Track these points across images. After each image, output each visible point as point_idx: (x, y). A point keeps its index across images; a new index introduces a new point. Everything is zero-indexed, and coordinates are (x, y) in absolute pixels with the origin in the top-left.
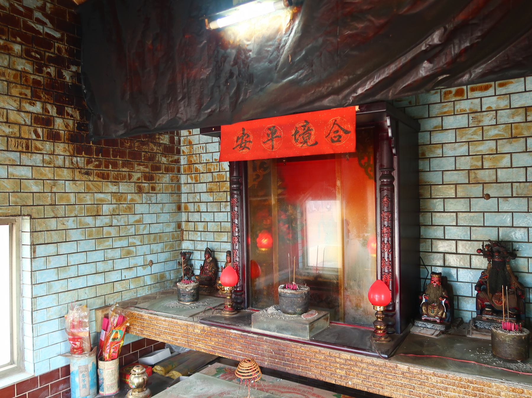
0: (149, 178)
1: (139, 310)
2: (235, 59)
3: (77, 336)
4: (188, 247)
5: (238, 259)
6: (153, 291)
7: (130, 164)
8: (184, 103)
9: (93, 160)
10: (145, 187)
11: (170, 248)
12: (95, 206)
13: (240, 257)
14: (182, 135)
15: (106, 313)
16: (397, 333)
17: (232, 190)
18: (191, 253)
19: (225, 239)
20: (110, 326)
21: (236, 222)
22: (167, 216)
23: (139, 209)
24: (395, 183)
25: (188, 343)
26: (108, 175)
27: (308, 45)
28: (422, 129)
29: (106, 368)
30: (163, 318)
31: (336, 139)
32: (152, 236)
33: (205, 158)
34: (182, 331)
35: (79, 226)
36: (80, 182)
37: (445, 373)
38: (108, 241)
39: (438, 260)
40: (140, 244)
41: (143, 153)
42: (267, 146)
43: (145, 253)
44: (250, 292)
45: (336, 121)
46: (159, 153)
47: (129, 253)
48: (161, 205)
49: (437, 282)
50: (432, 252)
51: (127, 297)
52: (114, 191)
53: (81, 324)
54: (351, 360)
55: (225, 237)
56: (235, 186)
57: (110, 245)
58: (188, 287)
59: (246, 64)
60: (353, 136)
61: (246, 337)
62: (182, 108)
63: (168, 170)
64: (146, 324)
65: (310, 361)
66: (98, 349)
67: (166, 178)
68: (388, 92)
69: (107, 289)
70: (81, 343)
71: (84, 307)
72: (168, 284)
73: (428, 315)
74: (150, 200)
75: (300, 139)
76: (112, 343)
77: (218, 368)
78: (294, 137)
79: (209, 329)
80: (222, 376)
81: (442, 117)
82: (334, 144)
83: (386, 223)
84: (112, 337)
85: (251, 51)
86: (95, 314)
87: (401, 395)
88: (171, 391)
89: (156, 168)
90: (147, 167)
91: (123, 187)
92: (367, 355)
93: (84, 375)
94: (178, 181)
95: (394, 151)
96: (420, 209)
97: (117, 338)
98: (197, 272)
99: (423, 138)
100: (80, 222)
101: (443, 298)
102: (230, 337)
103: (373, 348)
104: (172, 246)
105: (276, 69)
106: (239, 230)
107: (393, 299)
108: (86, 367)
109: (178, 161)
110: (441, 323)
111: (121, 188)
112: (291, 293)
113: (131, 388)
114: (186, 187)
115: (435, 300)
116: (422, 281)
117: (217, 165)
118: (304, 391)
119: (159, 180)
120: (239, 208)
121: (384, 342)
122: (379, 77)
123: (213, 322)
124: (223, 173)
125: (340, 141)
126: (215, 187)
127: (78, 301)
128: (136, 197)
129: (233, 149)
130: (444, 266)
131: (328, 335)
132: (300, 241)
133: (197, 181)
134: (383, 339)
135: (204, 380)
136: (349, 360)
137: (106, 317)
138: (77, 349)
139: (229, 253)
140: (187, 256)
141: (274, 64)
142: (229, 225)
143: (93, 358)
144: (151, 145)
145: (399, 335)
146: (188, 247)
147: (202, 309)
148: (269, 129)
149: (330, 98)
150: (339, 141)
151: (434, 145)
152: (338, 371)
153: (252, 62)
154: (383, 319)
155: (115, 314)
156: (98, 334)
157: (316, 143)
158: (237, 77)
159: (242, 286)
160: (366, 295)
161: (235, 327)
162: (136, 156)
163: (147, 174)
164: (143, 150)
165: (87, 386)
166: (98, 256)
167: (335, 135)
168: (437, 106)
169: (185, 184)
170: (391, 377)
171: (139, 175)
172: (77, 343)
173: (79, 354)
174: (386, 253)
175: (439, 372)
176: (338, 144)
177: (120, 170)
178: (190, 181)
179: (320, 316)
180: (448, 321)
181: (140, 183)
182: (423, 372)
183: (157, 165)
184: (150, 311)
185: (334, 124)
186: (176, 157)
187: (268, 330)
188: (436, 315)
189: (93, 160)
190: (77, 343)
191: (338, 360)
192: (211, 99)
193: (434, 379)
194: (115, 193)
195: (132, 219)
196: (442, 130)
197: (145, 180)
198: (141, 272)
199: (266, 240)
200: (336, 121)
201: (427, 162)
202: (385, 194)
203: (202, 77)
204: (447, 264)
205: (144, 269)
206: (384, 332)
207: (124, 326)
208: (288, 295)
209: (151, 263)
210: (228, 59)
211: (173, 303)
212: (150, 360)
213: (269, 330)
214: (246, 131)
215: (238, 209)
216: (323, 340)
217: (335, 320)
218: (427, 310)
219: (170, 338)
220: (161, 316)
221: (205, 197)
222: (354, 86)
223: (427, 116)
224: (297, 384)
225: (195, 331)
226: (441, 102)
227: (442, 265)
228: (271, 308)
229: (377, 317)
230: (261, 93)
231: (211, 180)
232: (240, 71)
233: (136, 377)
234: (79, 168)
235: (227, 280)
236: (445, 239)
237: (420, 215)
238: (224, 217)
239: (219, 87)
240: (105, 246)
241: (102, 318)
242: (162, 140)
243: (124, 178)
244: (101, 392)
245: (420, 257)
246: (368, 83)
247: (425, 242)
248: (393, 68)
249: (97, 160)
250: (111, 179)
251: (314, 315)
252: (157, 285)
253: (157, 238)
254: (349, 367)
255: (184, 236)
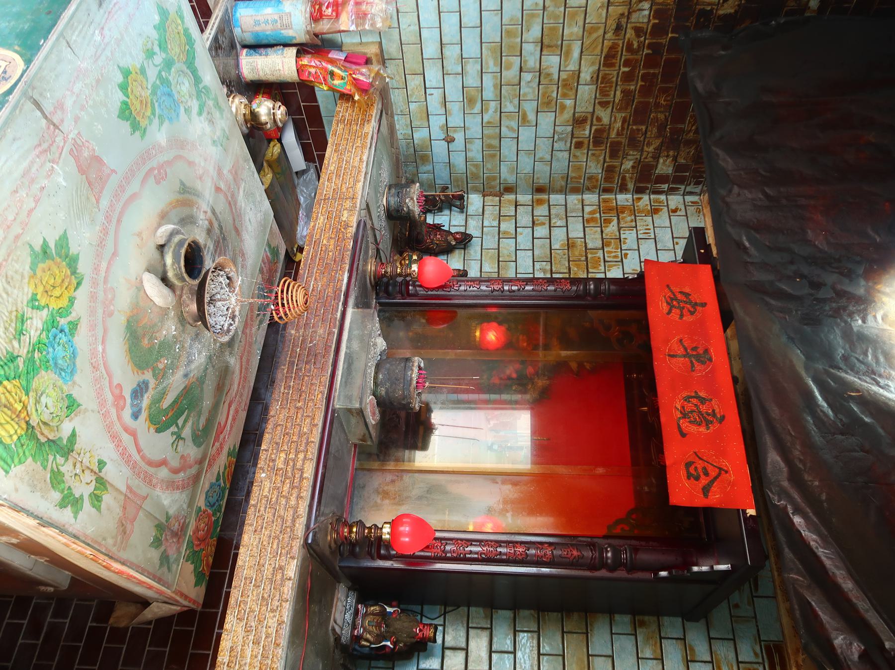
0: (599, 138)
1: (378, 117)
2: (849, 293)
3: (342, 10)
4: (472, 204)
5: (462, 288)
6: (402, 143)
7: (627, 105)
8: (760, 199)
9: (642, 39)
10: (584, 130)
11: (472, 174)
12: (560, 42)
13: (466, 293)
14: (670, 197)
15: (374, 60)
16: (341, 561)
17: (575, 281)
18: (462, 209)
19: (487, 268)
20: (354, 67)
21: (528, 288)
22: (528, 169)
23: (546, 120)
24: (603, 573)
25: (325, 200)
26: (612, 65)
27: (883, 428)
28: (688, 625)
29: (286, 60)
30: (365, 158)
31: (692, 470)
32: (495, 142)
33: (630, 237)
34: (344, 190)
35: (527, 14)
36: (604, 15)
37: (284, 642)
38: (495, 65)
39: (454, 638)
40: (485, 120)
41: (644, 128)
42: (675, 347)
43: (468, 129)
44: (407, 309)
45: (726, 472)
46: (641, 156)
47: (471, 101)
48: (548, 157)
49: (420, 635)
50: (468, 628)
51: (397, 97)
52: (582, 75)
53: (361, 16)
54: (302, 478)
55: (490, 268)
56: (592, 287)
57: (488, 68)
58: (413, 204)
59: (837, 313)
60: (699, 501)
61: (336, 297)
62: (750, 196)
63: (609, 171)
64: (355, 128)
65: (298, 408)
66: (315, 46)
67: (595, 169)
68: (799, 573)
69: (412, 63)
70: (329, 17)
71: (388, 23)
72: (411, 168)
73: (366, 615)
74: (559, 139)
75: (689, 407)
76: (326, 69)
77: (278, 250)
78: (693, 394)
79: (349, 235)
80: (267, 256)
81: (712, 662)
82: (683, 467)
83: (533, 551)
84: (336, 70)
85: (864, 322)
86: (373, 43)
87: (245, 562)
88: (249, 168)
89: (615, 151)
90: (618, 134)
91: (586, 92)
92: (311, 506)
93: (277, 22)
94: (588, 189)
95: (663, 574)
96: (543, 611)
97: (332, 77)
98: (430, 219)
99: (672, 626)
100: (533, 16)
101: (395, 644)
102: (337, 271)
103: (322, 519)
104: (475, 176)
105: (832, 367)
106: (514, 291)
107: (400, 557)
108: (289, 26)
109: (623, 189)
110: (352, 636)
111: (587, 87)
112: (411, 379)
113: (250, 102)
114: (576, 202)
115: (391, 629)
116: (418, 608)
117: (615, 257)
118: (241, 395)
119: (593, 155)
120: (553, 293)
121: (329, 538)
122: (827, 557)
123: (361, 243)
124: (602, 268)
125: (689, 478)
126: (577, 253)
127: (398, 12)
128: (567, 115)
129: (668, 286)
130: (444, 648)
131: (340, 440)
132: (505, 397)
133: (588, 221)
134: (335, 536)
135: (263, 226)
136: (301, 476)
137: (368, 61)
138: (320, 10)
139: (464, 273)
140: (456, 202)
141: (842, 365)
142: (511, 274)
143: (302, 38)
144: (657, 142)
145: (337, 564)
146: (472, 204)
147: (377, 226)
148: (706, 351)
149: (782, 465)
150: (689, 476)
151: (658, 644)
152: (283, 455)
153: (843, 324)
154: (368, 538)
155: (372, 75)
156: (339, 47)
157: (683, 435)
158: (811, 295)
159: (415, 295)
160: (404, 510)
161: (353, 280)
162: (641, 114)
163: (605, 135)
164: (650, 128)
165: (257, 28)
166: (471, 48)
167: (700, 470)
168: (732, 655)
169: (583, 200)
170: (275, 546)
171: (606, 120)
172: (330, 10)
173: (311, 13)
174: (479, 549)
175: (286, 631)
176: (683, 473)
177: (618, 87)
178: (587, 209)
179: (371, 429)
180: (354, 649)
181: (592, 121)
182: (284, 604)
183: (621, 153)
184: (375, 136)
185: (720, 469)
186: (631, 186)
187: (349, 337)
188: (365, 630)
189: (642, 39)
190: (330, 10)
191: (301, 456)
192: (769, 247)
193: (273, 622)
194: (579, 77)
195: (529, 108)
196: (688, 661)
197: (596, 130)
198: (437, 122)
199: (493, 338)
200: (726, 472)
201: (629, 630)
202: (585, 554)
203: (809, 231)
204: (447, 652)
205: (441, 128)
206: (346, 538)
207: (353, 90)
208: (409, 373)
209: (450, 140)
210: (846, 281)
211: (386, 176)
212: (290, 137)
213: (349, 340)
214: (699, 308)
215: (551, 291)
216: (333, 433)
217: (359, 453)
218: (373, 614)
219: (332, 168)
220: (369, 155)
221: (559, 235)
222: (808, 510)
223: (712, 635)
224: (252, 384)
225: (345, 212)
226: (738, 662)
227: (447, 645)
228: (384, 343)
229: (370, 528)
230: (784, 339)
231: (590, 246)
232: (824, 301)
233: (270, 110)
234: (629, 13)
235: (429, 269)
236: (491, 652)
237: (532, 612)
238: (525, 267)
239: (792, 263)
240: (486, 60)
241: (365, 54)
242: (665, 161)
243: (603, 92)
244: (245, 51)
245: (459, 607)
246: (814, 537)
247: (486, 617)
248: (848, 585)
249: (641, 45)
250: (605, 70)
251: (373, 419)
252: (412, 149)
253: (492, 150)
254: (290, 474)
255: (491, 198)
